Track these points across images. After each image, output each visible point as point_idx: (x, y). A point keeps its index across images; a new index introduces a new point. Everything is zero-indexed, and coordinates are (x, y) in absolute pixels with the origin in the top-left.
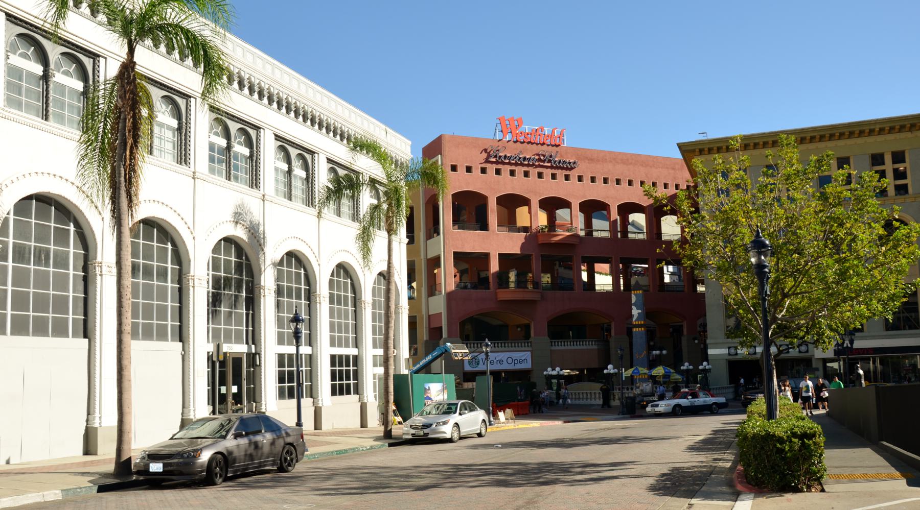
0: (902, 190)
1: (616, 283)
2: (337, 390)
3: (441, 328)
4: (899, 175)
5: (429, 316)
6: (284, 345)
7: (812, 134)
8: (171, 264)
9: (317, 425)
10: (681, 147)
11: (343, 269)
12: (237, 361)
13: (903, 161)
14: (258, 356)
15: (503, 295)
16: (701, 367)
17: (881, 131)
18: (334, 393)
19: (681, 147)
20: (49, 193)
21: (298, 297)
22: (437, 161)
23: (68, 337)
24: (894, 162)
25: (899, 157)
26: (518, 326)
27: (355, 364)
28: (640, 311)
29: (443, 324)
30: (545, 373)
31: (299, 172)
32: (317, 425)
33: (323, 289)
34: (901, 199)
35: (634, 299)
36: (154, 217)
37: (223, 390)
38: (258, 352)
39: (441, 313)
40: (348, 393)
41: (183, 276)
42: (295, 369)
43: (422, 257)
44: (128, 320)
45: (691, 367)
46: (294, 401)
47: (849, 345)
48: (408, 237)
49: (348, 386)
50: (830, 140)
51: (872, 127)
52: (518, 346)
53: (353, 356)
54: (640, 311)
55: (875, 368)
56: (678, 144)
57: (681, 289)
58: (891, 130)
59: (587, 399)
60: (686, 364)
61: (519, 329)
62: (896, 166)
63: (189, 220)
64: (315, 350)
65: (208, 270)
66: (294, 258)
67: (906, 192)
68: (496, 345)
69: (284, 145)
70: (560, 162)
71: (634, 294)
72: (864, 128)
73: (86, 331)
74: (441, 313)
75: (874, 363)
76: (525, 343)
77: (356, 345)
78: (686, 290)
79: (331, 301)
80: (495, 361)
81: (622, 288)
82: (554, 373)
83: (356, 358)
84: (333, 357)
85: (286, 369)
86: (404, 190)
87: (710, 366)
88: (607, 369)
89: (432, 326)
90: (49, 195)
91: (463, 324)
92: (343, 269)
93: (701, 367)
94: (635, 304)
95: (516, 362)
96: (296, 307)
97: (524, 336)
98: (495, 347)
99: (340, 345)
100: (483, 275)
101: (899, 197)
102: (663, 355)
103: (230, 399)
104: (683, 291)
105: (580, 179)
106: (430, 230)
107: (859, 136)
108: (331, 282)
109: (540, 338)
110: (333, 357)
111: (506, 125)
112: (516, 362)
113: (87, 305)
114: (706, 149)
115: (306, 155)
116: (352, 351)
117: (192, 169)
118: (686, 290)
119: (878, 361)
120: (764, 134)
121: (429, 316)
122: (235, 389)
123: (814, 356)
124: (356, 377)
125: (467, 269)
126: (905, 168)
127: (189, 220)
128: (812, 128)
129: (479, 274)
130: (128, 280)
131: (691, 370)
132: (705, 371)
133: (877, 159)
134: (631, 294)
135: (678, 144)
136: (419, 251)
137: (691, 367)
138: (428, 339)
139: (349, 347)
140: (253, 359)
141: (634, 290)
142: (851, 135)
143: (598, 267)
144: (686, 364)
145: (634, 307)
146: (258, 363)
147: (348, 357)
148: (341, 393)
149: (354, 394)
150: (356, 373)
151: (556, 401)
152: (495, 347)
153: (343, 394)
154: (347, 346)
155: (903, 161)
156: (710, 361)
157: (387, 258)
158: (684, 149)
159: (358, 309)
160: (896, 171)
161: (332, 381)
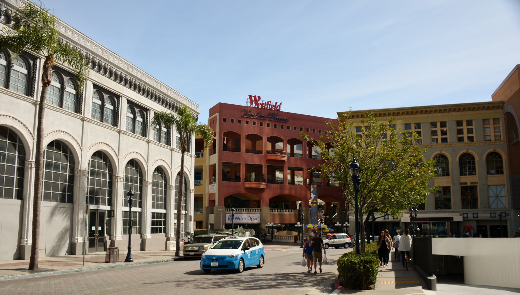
0: (444, 140)
1: (305, 181)
2: (154, 231)
3: (215, 201)
4: (444, 133)
5: (209, 194)
6: (137, 207)
7: (403, 111)
8: (46, 159)
9: (143, 248)
10: (339, 114)
11: (159, 170)
12: (102, 213)
13: (446, 126)
14: (113, 212)
15: (247, 185)
16: (344, 225)
17: (435, 111)
18: (153, 232)
19: (339, 114)
20: (6, 125)
21: (136, 183)
22: (216, 117)
23: (13, 199)
24: (441, 127)
25: (443, 124)
26: (254, 201)
27: (165, 218)
28: (315, 196)
29: (216, 198)
30: (266, 225)
31: (139, 119)
32: (143, 248)
33: (149, 178)
34: (444, 144)
35: (312, 190)
36: (61, 139)
37: (93, 228)
38: (113, 209)
39: (215, 193)
40: (161, 232)
41: (26, 161)
42: (128, 219)
43: (207, 164)
44: (42, 191)
45: (340, 225)
46: (128, 235)
47: (415, 216)
48: (196, 154)
49: (161, 229)
50: (420, 114)
51: (431, 109)
52: (254, 211)
53: (164, 213)
54: (315, 196)
55: (430, 227)
56: (337, 113)
57: (320, 184)
58: (440, 111)
59: (288, 239)
60: (338, 223)
61: (255, 203)
62: (442, 129)
63: (79, 141)
64: (143, 210)
65: (89, 167)
66: (133, 163)
67: (447, 142)
68: (237, 210)
69: (132, 105)
70: (278, 119)
71: (312, 187)
72: (427, 109)
73: (20, 195)
74: (215, 193)
75: (429, 225)
76: (257, 210)
77: (165, 208)
78: (322, 185)
79: (154, 185)
80: (242, 218)
81: (308, 184)
82: (271, 225)
83: (165, 214)
84: (153, 214)
85: (159, 227)
86: (504, 157)
87: (349, 225)
88: (297, 224)
89: (210, 200)
90: (6, 126)
91: (226, 199)
92: (159, 170)
93: (344, 225)
94: (312, 192)
95: (252, 219)
96: (131, 188)
97: (257, 205)
98: (237, 211)
99: (157, 208)
100: (238, 174)
101: (443, 144)
102: (327, 218)
103: (97, 234)
104: (321, 185)
105: (288, 128)
106: (211, 150)
107: (439, 112)
108: (154, 175)
109: (266, 209)
110: (153, 214)
111: (254, 99)
112: (252, 219)
113: (21, 183)
114: (360, 115)
115: (144, 110)
116: (163, 211)
117: (82, 115)
118: (322, 185)
119: (431, 224)
120: (380, 110)
121: (209, 194)
122: (100, 228)
123: (400, 221)
124: (165, 225)
125: (230, 171)
126: (447, 130)
127: (79, 141)
128: (403, 108)
129: (236, 174)
130: (43, 170)
131: (340, 226)
132: (347, 227)
133: (434, 124)
134: (311, 187)
135: (337, 113)
136: (206, 161)
137: (340, 225)
138: (208, 206)
139: (162, 209)
140: (111, 214)
141: (312, 185)
142: (421, 112)
143: (296, 172)
144: (338, 223)
145: (312, 194)
146: (113, 215)
147: (161, 214)
148: (157, 232)
149: (15, 199)
150: (165, 222)
151: (271, 240)
152: (237, 211)
153: (158, 233)
154: (161, 208)
155: (446, 126)
156: (350, 222)
157: (180, 164)
158: (340, 115)
159: (188, 193)
160: (442, 131)
161: (152, 226)
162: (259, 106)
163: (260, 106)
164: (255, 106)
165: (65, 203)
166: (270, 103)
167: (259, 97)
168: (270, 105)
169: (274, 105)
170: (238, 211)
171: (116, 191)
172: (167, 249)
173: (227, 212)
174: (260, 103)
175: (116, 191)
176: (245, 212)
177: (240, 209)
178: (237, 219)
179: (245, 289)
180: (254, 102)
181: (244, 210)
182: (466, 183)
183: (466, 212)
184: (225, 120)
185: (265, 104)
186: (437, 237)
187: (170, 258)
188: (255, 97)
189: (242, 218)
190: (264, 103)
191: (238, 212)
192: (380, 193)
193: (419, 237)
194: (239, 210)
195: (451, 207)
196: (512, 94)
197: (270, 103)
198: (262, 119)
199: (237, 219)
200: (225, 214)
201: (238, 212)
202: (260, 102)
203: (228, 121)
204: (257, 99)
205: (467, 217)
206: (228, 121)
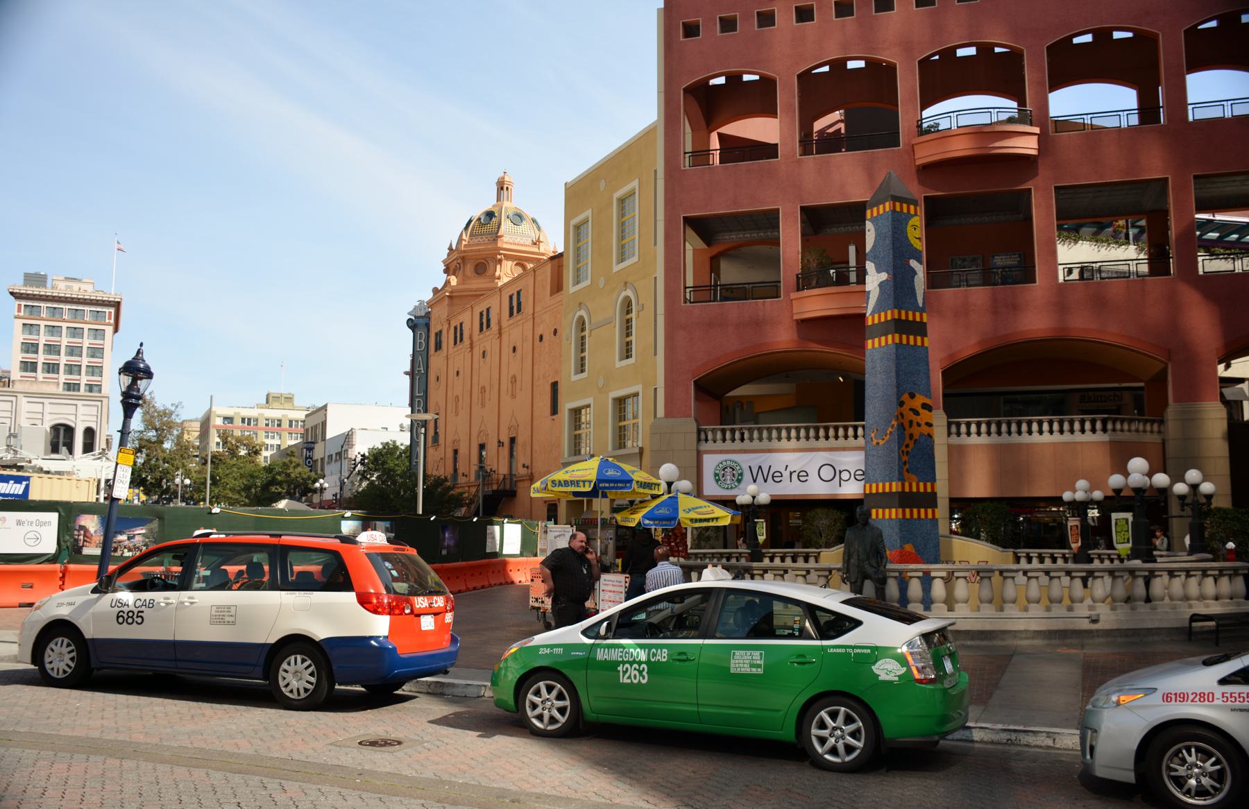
80: (786, 474)
170: (846, 437)
171: (682, 139)
172: (735, 528)
173: (704, 446)
175: (682, 139)
176: (793, 443)
177: (836, 429)
178: (760, 478)
179: (94, 459)
181: (793, 433)
186: (933, 487)
187: (1130, 580)
189: (786, 474)
191: (812, 441)
192: (160, 496)
193: (542, 480)
194: (841, 432)
195: (801, 210)
199: (760, 478)
200: (699, 455)
201: (812, 440)
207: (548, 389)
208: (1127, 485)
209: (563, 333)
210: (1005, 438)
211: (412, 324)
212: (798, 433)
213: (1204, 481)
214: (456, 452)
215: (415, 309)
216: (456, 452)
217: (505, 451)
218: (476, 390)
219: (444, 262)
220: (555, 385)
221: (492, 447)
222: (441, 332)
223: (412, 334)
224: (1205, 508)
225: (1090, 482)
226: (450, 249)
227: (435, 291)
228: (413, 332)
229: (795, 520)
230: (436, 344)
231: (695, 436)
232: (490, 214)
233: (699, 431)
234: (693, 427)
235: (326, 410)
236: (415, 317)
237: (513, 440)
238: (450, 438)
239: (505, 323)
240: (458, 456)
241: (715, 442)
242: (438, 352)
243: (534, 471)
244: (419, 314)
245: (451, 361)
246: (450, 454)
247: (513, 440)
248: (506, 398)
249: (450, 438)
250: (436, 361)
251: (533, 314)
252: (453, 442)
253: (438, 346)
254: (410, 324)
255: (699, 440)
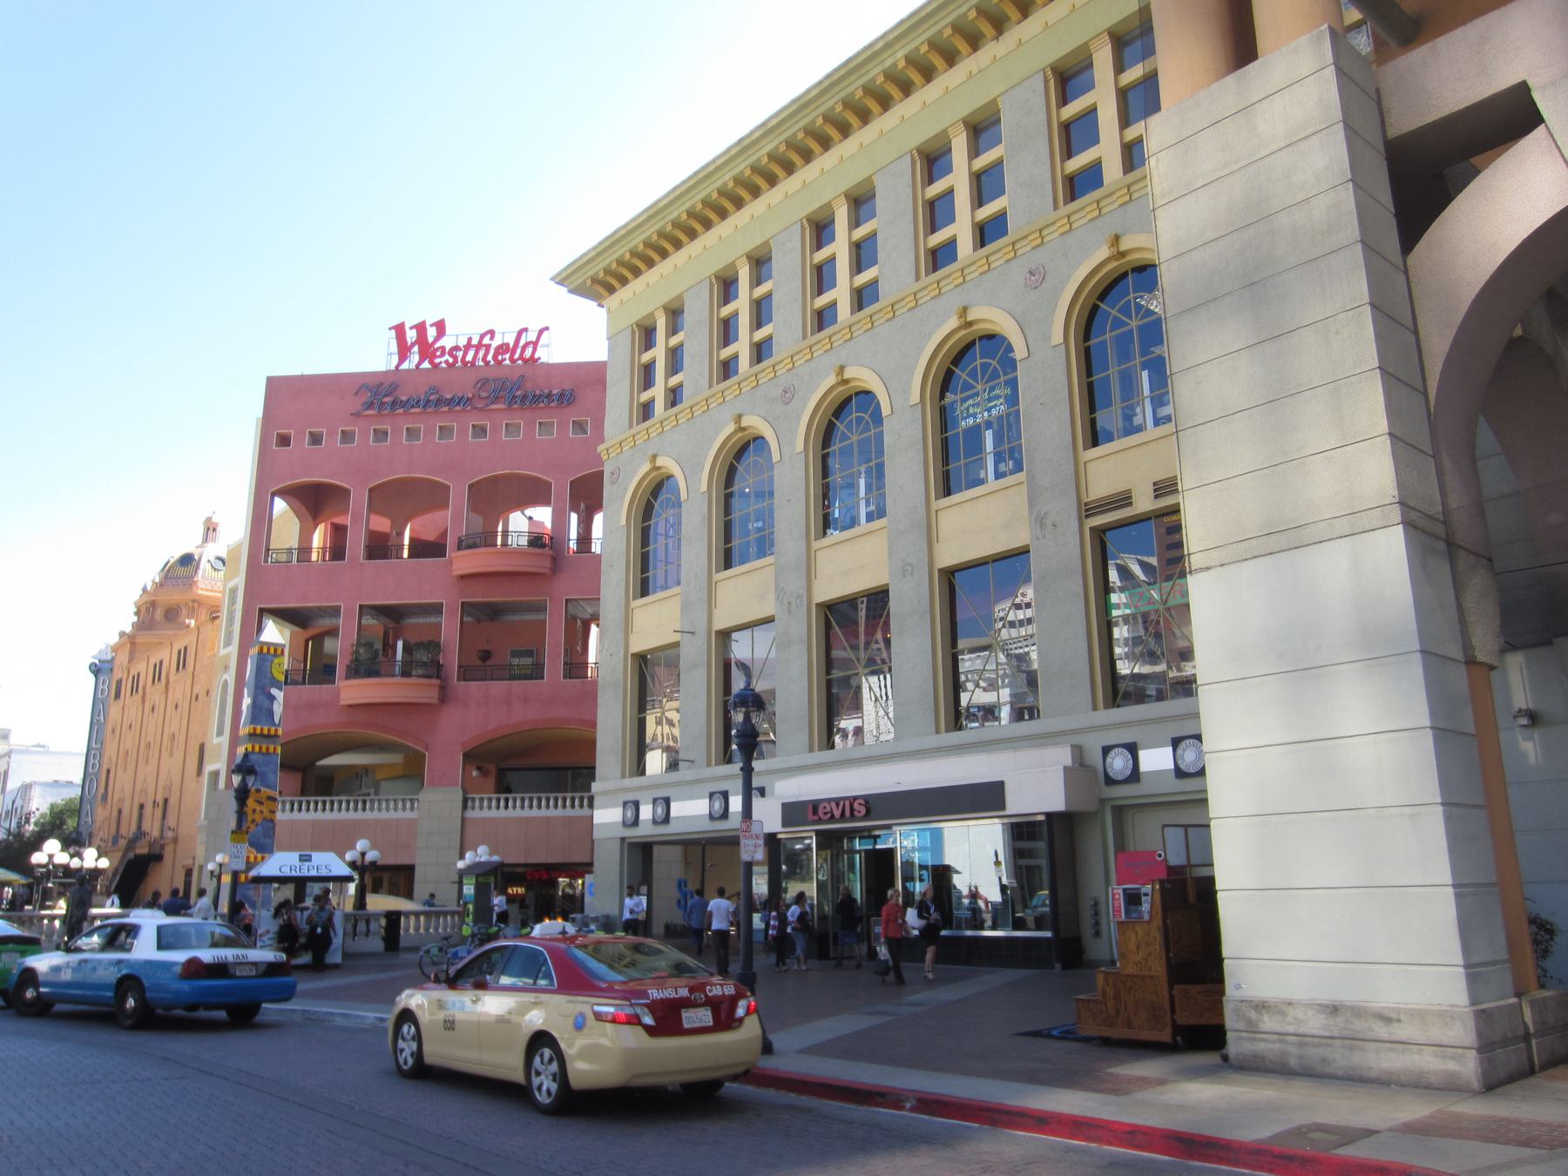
56: (562, 279)
70: (525, 397)
135: (562, 279)
162: (437, 361)
163: (441, 360)
164: (421, 361)
165: (637, 712)
166: (492, 338)
167: (440, 327)
168: (488, 347)
169: (508, 345)
174: (443, 348)
180: (416, 349)
182: (1124, 500)
183: (1127, 736)
184: (284, 441)
185: (468, 346)
188: (421, 328)
190: (462, 342)
196: (1438, 219)
197: (492, 338)
198: (446, 409)
202: (447, 342)
203: (300, 443)
204: (431, 333)
205: (1135, 775)
206: (300, 443)
207: (197, 748)
208: (82, 866)
209: (213, 694)
210: (569, 812)
211: (96, 670)
212: (380, 805)
213: (215, 861)
214: (120, 811)
215: (100, 652)
216: (120, 811)
217: (159, 812)
218: (142, 745)
219: (135, 603)
220: (202, 747)
221: (148, 808)
222: (121, 680)
223: (94, 679)
224: (77, 887)
225: (380, 852)
226: (144, 590)
227: (122, 634)
228: (96, 676)
229: (386, 877)
230: (116, 693)
231: (460, 804)
232: (187, 560)
233: (465, 801)
234: (457, 795)
235: (10, 757)
236: (100, 661)
237: (166, 801)
238: (116, 797)
239: (172, 678)
240: (143, 811)
241: (380, 811)
242: (118, 701)
243: (179, 835)
244: (104, 657)
245: (126, 712)
246: (115, 814)
247: (166, 801)
248: (165, 755)
249: (116, 797)
250: (115, 711)
251: (193, 673)
252: (119, 801)
253: (118, 695)
254: (93, 668)
255: (465, 807)
